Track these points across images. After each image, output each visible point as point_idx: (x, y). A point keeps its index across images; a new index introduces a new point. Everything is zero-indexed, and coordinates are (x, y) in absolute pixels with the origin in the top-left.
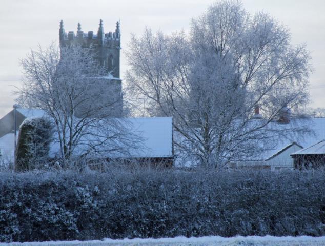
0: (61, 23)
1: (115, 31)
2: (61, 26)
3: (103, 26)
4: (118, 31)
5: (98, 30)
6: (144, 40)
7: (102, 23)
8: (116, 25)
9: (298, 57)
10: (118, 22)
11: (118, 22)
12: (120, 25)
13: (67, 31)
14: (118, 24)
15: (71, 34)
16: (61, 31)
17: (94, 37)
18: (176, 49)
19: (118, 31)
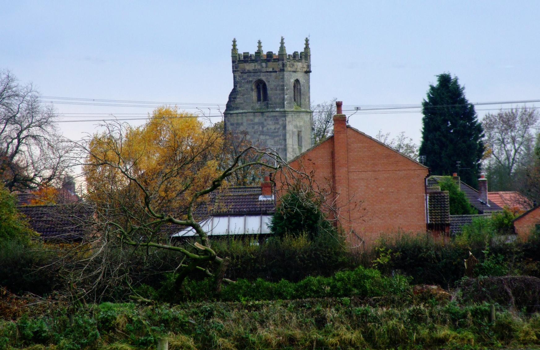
0: (234, 41)
1: (303, 50)
2: (234, 45)
3: (285, 45)
4: (307, 47)
5: (278, 49)
6: (476, 120)
7: (284, 41)
8: (232, 43)
9: (506, 243)
10: (307, 38)
11: (307, 38)
12: (310, 42)
13: (241, 51)
14: (307, 41)
15: (270, 54)
16: (234, 49)
17: (493, 169)
18: (290, 338)
19: (307, 47)
